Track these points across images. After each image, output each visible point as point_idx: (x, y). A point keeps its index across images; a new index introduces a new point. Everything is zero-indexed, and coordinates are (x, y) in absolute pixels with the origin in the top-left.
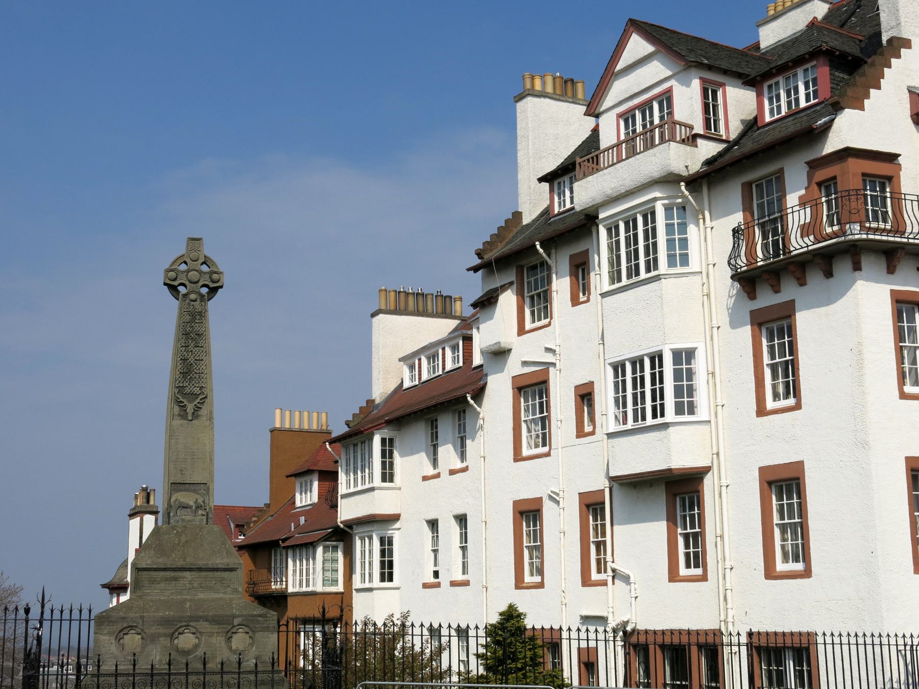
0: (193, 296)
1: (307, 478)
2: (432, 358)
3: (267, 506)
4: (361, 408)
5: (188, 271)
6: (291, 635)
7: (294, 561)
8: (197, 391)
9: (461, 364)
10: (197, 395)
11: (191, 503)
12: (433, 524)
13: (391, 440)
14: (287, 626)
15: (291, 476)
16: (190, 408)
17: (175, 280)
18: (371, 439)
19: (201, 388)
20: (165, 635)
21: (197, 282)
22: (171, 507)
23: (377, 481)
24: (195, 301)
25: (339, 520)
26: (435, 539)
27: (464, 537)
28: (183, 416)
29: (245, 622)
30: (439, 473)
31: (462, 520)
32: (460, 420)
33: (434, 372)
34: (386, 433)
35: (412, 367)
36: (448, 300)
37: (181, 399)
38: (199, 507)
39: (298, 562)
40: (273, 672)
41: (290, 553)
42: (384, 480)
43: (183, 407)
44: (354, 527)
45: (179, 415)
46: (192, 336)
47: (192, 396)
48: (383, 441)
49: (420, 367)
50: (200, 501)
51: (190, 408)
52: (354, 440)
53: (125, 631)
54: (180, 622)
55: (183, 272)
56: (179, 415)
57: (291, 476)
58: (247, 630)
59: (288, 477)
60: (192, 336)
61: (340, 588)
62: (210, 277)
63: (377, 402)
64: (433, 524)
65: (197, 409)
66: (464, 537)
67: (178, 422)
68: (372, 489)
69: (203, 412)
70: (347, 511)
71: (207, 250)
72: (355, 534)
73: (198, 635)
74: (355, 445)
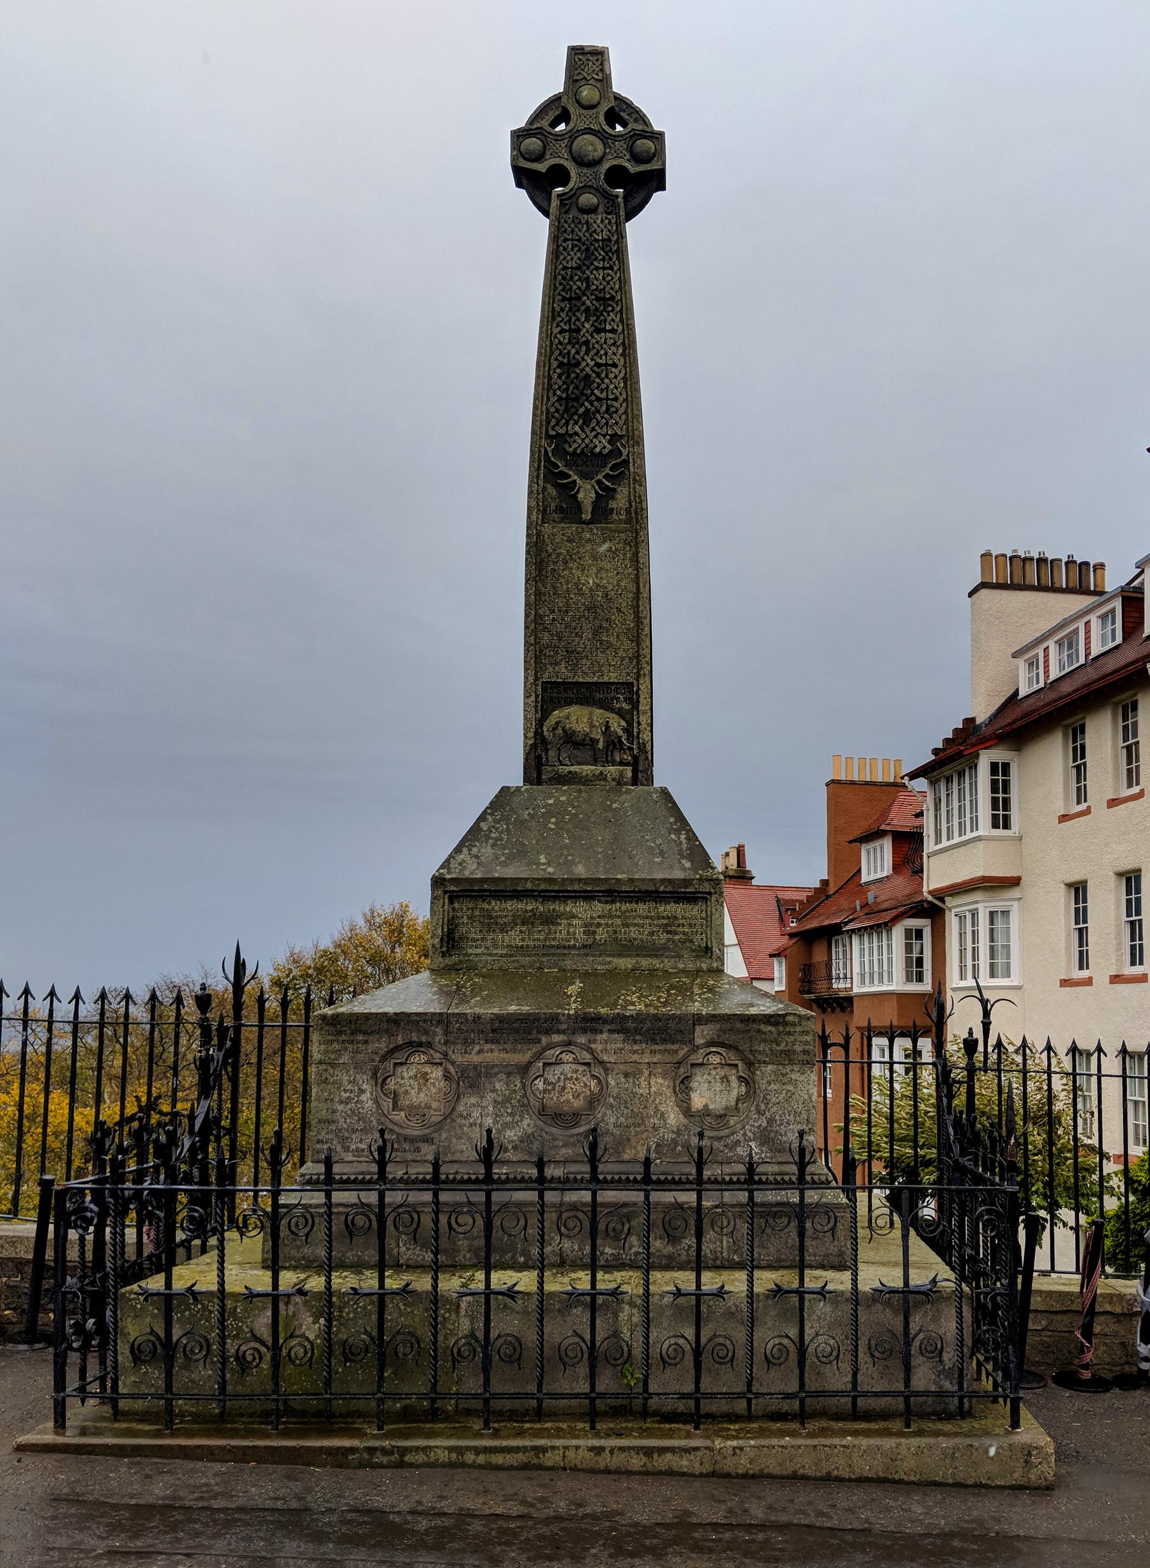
0: (588, 199)
1: (877, 844)
2: (1069, 642)
3: (825, 883)
4: (956, 730)
5: (572, 135)
6: (854, 1070)
7: (861, 943)
8: (602, 445)
9: (1119, 639)
10: (602, 458)
11: (597, 735)
12: (1079, 890)
13: (1006, 767)
14: (846, 1047)
15: (855, 841)
16: (586, 494)
17: (539, 158)
18: (974, 767)
19: (614, 438)
20: (510, 1071)
21: (599, 162)
22: (544, 741)
23: (985, 827)
24: (592, 210)
25: (925, 889)
26: (1081, 915)
27: (1134, 907)
28: (570, 510)
29: (725, 1038)
30: (1089, 808)
31: (1131, 880)
32: (1125, 718)
33: (1070, 663)
34: (998, 755)
35: (1032, 664)
36: (1084, 567)
37: (562, 468)
38: (614, 743)
39: (866, 946)
40: (802, 1182)
41: (855, 940)
42: (995, 825)
43: (568, 490)
44: (947, 899)
45: (559, 510)
46: (586, 313)
47: (588, 461)
48: (994, 767)
49: (1046, 661)
50: (617, 725)
51: (586, 494)
52: (946, 771)
53: (400, 1057)
54: (548, 1032)
55: (561, 135)
56: (559, 510)
57: (855, 841)
58: (733, 1058)
59: (850, 842)
60: (586, 313)
61: (926, 986)
62: (631, 150)
63: (978, 722)
64: (1079, 890)
65: (605, 495)
66: (1134, 907)
67: (554, 531)
68: (979, 839)
69: (620, 501)
70: (938, 874)
71: (624, 82)
72: (950, 909)
73: (598, 1071)
74: (949, 780)
